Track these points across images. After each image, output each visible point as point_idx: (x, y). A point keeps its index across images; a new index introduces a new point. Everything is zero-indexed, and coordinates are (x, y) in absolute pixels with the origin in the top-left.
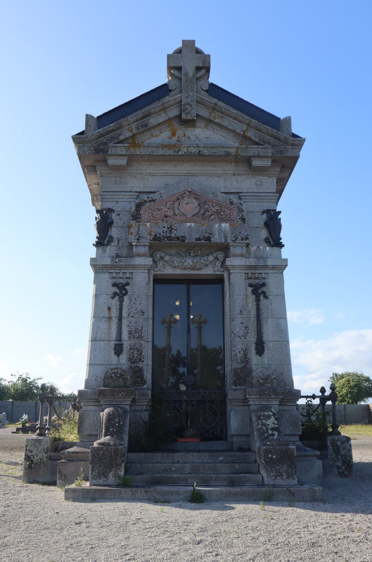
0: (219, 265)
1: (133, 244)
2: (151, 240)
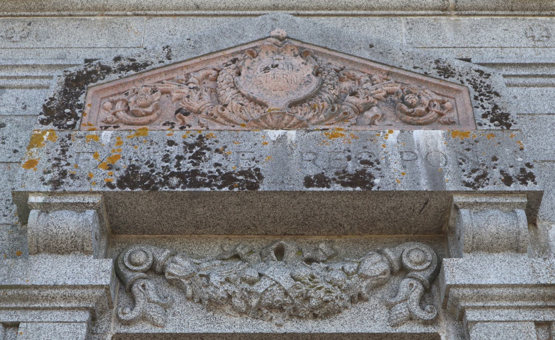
0: (416, 295)
1: (32, 199)
2: (109, 184)
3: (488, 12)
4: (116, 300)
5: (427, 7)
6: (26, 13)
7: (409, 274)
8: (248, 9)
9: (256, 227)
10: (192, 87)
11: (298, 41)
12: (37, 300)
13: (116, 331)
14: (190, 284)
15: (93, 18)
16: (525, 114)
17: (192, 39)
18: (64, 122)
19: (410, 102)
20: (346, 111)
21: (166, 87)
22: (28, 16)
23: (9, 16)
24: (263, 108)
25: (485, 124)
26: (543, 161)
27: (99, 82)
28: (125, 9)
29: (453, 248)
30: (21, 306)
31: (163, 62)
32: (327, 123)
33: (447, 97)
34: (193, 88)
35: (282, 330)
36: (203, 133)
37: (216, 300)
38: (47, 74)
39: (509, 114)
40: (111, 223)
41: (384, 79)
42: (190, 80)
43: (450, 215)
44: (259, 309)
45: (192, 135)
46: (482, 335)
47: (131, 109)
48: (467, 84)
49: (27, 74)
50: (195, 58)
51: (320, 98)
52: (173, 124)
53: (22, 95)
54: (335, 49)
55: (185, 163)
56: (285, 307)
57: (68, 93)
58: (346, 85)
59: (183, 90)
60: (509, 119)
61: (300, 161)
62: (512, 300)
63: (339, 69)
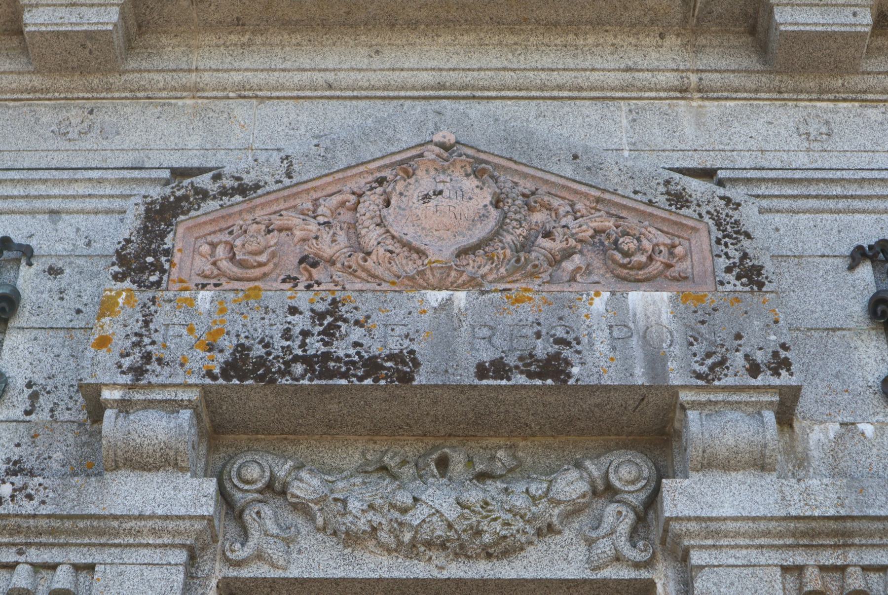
0: (624, 527)
1: (106, 394)
2: (210, 374)
3: (745, 95)
4: (221, 530)
5: (658, 87)
6: (86, 95)
7: (618, 497)
8: (403, 88)
9: (411, 427)
10: (322, 222)
11: (472, 147)
12: (117, 535)
13: (222, 575)
14: (321, 510)
15: (180, 102)
16: (789, 256)
17: (321, 146)
18: (145, 277)
19: (626, 248)
20: (537, 262)
21: (286, 222)
22: (88, 99)
23: (62, 99)
24: (420, 258)
25: (729, 283)
26: (809, 330)
27: (193, 213)
28: (226, 89)
29: (678, 459)
30: (97, 542)
31: (281, 182)
32: (510, 279)
33: (679, 237)
34: (325, 223)
35: (445, 574)
36: (339, 295)
37: (357, 533)
38: (118, 193)
39: (762, 267)
40: (212, 421)
41: (592, 208)
42: (320, 210)
43: (675, 413)
44: (414, 546)
45: (322, 299)
46: (710, 585)
47: (238, 258)
48: (706, 218)
49: (91, 192)
50: (326, 175)
51: (501, 241)
52: (295, 279)
53: (84, 223)
54: (524, 161)
55: (313, 341)
56: (448, 544)
57: (151, 232)
58: (539, 217)
59: (309, 227)
60: (762, 274)
61: (471, 340)
62: (752, 537)
63: (529, 193)
